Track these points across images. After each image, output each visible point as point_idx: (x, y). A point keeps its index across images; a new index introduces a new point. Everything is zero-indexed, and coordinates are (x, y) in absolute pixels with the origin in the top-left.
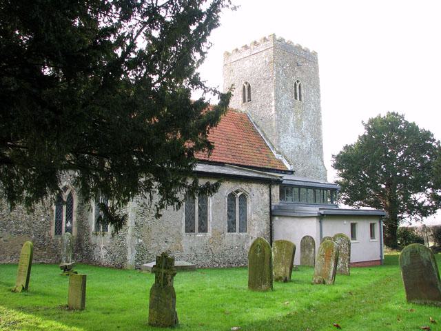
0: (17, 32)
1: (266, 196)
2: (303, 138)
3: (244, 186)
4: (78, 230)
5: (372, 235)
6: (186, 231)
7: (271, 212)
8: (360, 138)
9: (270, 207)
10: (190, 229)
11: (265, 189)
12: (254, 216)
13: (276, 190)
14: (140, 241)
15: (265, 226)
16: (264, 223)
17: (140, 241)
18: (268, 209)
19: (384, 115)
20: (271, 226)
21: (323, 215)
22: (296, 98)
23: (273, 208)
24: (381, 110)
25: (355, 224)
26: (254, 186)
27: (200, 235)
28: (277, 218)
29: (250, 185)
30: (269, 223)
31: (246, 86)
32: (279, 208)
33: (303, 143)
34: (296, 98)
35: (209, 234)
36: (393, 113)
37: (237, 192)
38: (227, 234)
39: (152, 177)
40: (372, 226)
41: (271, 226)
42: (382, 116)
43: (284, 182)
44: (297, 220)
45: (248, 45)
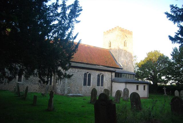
0: (40, 33)
1: (110, 76)
2: (127, 58)
3: (103, 73)
4: (53, 84)
5: (144, 89)
6: (84, 85)
7: (112, 80)
8: (145, 58)
9: (111, 79)
10: (85, 84)
11: (110, 73)
12: (106, 82)
13: (114, 74)
14: (69, 87)
15: (109, 85)
16: (109, 84)
17: (69, 87)
18: (111, 80)
19: (153, 51)
20: (111, 85)
21: (126, 82)
22: (125, 46)
23: (112, 79)
24: (152, 49)
25: (138, 85)
26: (106, 73)
27: (88, 87)
28: (113, 83)
29: (105, 72)
30: (111, 84)
31: (110, 42)
32: (114, 80)
33: (127, 60)
34: (125, 46)
35: (91, 86)
36: (156, 51)
37: (101, 74)
38: (97, 87)
39: (181, 14)
40: (144, 86)
41: (111, 85)
42: (153, 51)
43: (116, 72)
44: (119, 83)
45: (111, 30)
